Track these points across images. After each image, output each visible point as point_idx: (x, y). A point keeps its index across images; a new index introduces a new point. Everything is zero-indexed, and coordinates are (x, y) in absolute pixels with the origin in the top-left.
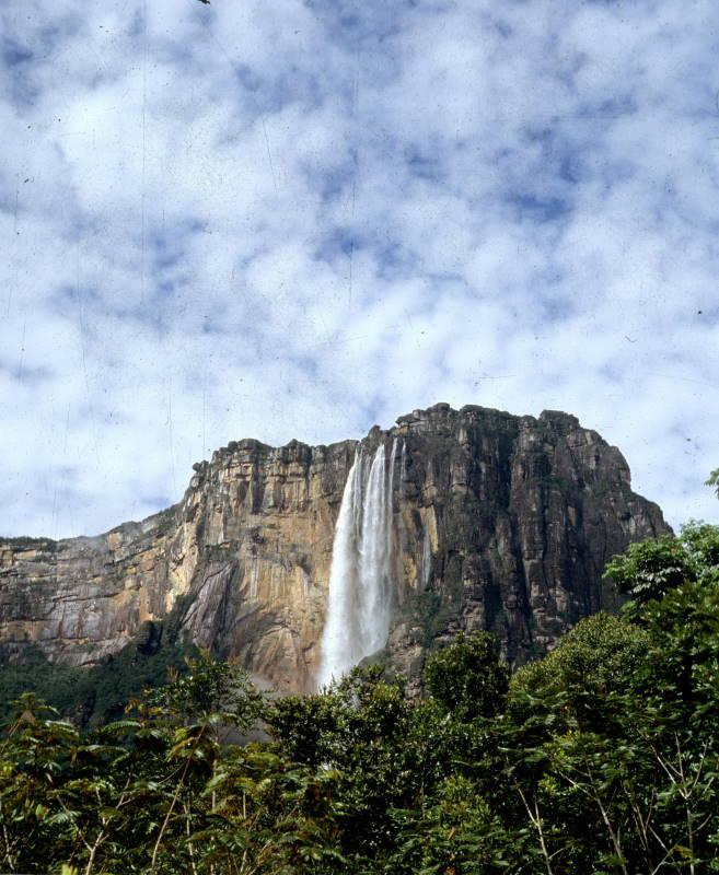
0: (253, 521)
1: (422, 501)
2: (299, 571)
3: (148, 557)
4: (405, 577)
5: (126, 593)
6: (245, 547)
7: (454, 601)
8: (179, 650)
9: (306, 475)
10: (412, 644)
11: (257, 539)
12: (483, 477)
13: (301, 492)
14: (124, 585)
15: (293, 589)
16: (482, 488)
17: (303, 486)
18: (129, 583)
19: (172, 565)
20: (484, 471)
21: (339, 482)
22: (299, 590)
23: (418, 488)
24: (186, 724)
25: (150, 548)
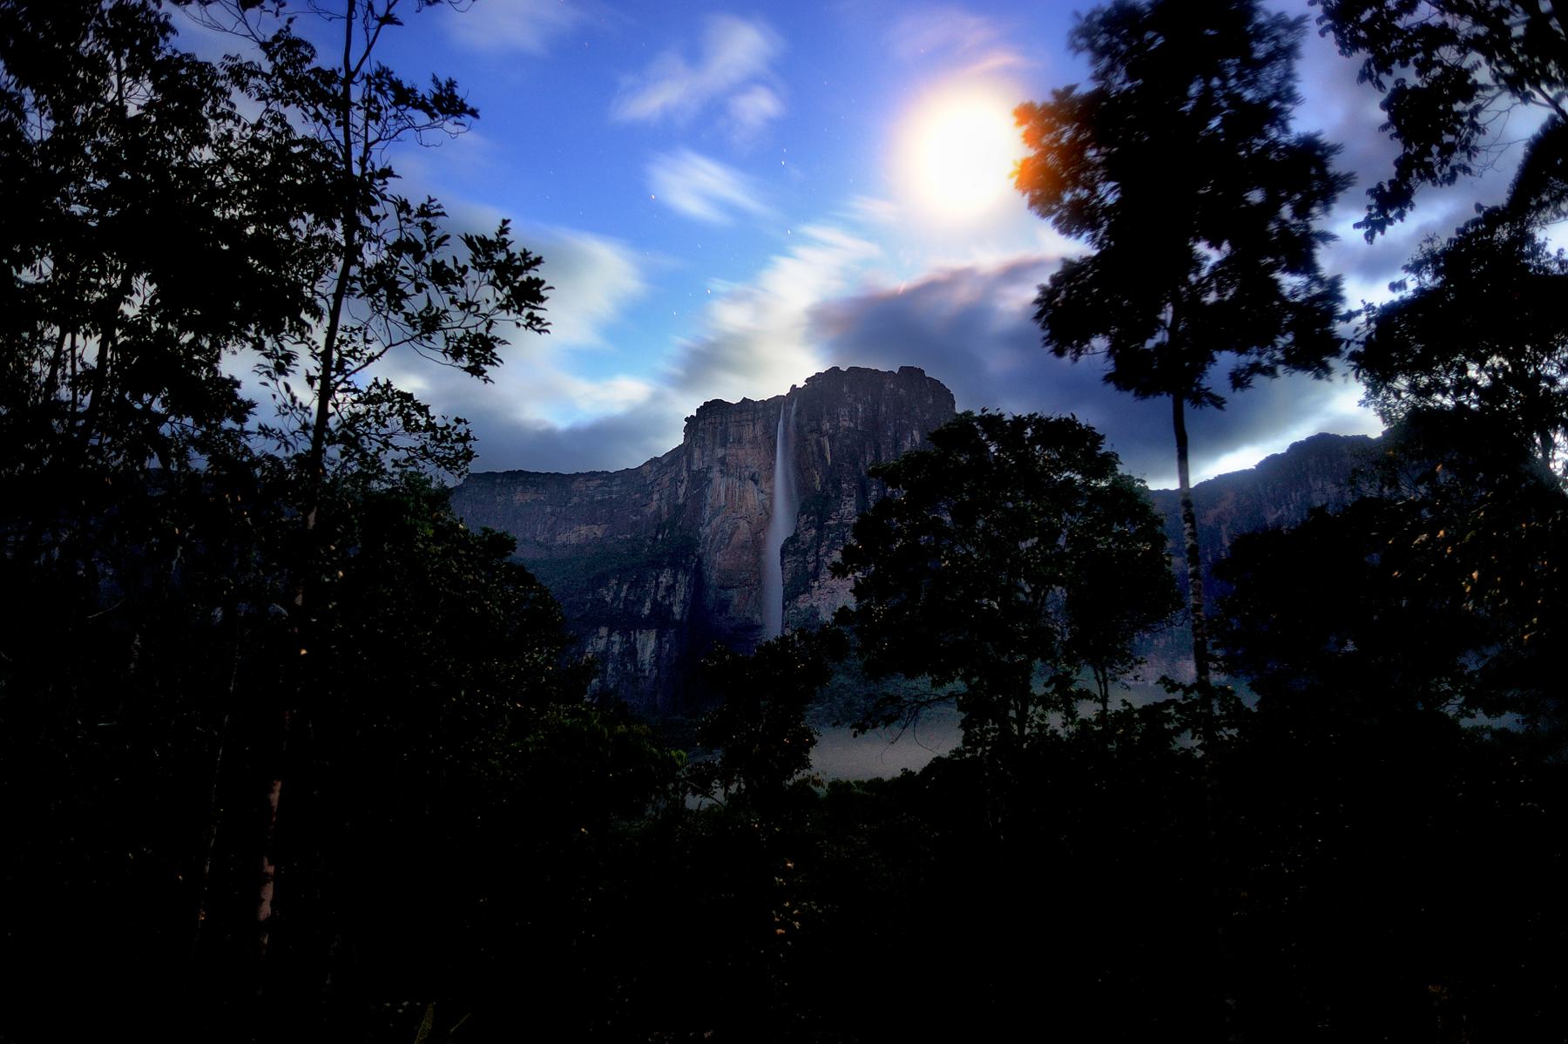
0: (720, 452)
1: (821, 433)
2: (751, 483)
3: (666, 478)
4: (416, 304)
5: (654, 503)
6: (716, 468)
7: (835, 497)
8: (719, 577)
9: (753, 420)
10: (810, 528)
11: (722, 461)
12: (860, 414)
13: (750, 431)
14: (367, 228)
15: (748, 495)
16: (859, 421)
17: (751, 427)
18: (656, 497)
19: (679, 484)
20: (860, 410)
21: (773, 424)
22: (752, 495)
23: (819, 425)
24: (475, 325)
25: (667, 473)
